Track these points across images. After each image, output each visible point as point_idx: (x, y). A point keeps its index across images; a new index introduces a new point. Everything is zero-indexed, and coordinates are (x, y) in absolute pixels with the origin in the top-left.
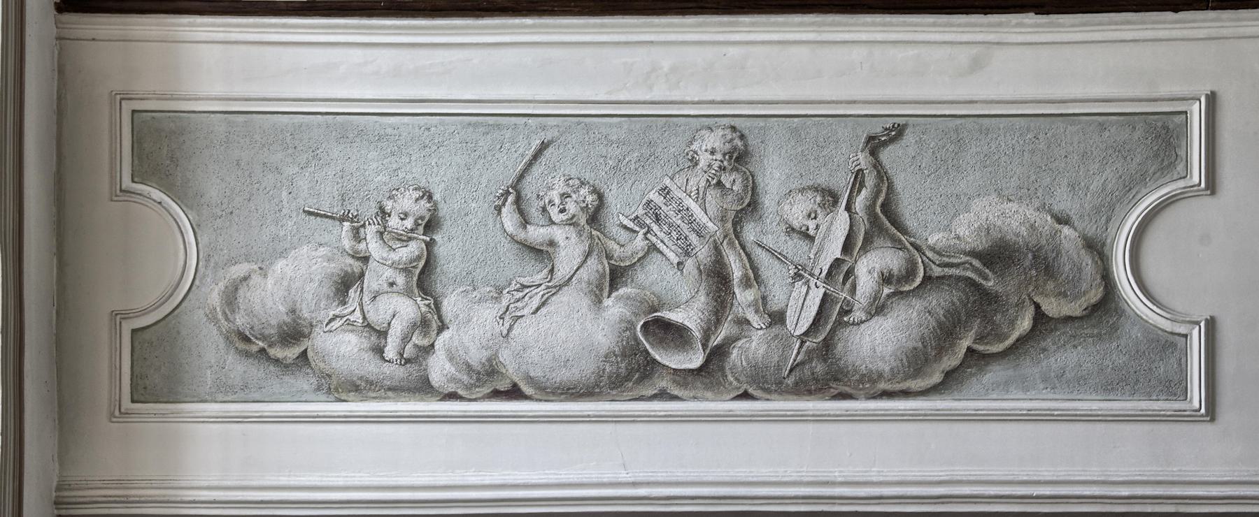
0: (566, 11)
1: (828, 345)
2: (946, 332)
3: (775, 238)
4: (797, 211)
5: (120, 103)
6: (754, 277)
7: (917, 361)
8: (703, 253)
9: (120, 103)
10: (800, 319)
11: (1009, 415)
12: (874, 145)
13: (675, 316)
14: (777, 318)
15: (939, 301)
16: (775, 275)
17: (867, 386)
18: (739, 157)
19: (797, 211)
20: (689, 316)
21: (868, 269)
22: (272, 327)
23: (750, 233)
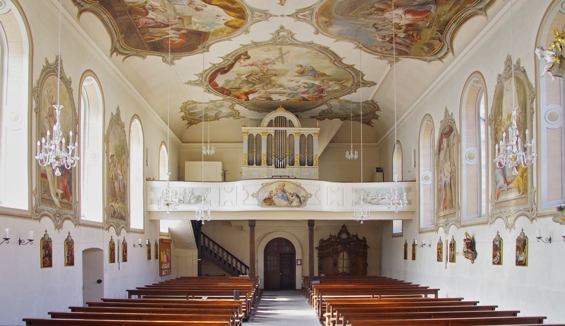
0: (466, 11)
1: (190, 201)
2: (196, 201)
3: (187, 195)
4: (188, 193)
5: (290, 274)
6: (186, 197)
7: (195, 202)
8: (183, 196)
9: (290, 274)
10: (188, 200)
11: (416, 310)
12: (192, 189)
13: (181, 199)
14: (187, 200)
15: (196, 199)
16: (187, 197)
17: (322, 275)
18: (185, 190)
19: (188, 193)
20: (182, 199)
21: (192, 197)
22: (242, 58)
23: (186, 194)
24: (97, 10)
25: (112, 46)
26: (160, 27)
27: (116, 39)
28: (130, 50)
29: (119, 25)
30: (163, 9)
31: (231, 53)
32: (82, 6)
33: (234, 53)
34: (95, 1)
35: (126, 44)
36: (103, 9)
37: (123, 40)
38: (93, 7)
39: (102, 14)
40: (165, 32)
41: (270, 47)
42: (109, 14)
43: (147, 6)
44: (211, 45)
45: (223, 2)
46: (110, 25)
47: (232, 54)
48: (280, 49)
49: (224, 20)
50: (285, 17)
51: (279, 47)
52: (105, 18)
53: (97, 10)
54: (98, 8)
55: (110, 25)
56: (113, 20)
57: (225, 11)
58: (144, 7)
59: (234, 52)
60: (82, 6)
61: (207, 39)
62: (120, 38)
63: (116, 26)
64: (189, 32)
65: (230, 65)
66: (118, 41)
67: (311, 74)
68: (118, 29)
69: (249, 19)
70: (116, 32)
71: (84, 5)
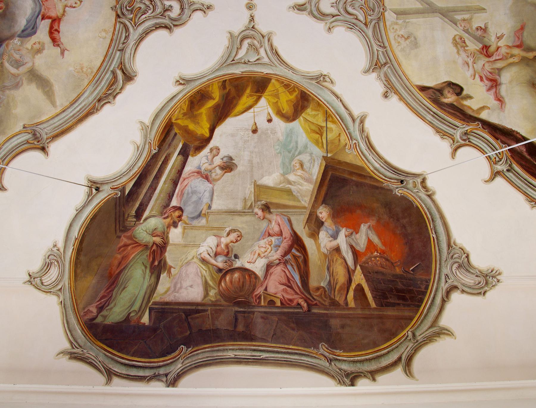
24: (202, 358)
25: (333, 377)
26: (306, 261)
27: (324, 363)
28: (389, 352)
29: (276, 337)
30: (228, 234)
31: (430, 124)
32: (166, 375)
33: (429, 117)
34: (177, 352)
35: (364, 350)
36: (208, 348)
37: (338, 352)
38: (190, 360)
39: (221, 356)
40: (326, 256)
41: (391, 36)
42: (230, 344)
43: (220, 262)
44: (386, 162)
45: (201, 113)
46: (264, 355)
47: (436, 123)
48: (400, 13)
49: (270, 121)
50: (247, 14)
51: (390, 16)
52: (235, 355)
53: (202, 358)
54: (197, 354)
55: (264, 355)
56: (254, 343)
57: (240, 107)
58: (223, 273)
59: (423, 118)
60: (166, 375)
61: (362, 168)
62: (327, 354)
63: (278, 345)
64: (324, 202)
65: (497, 135)
66: (330, 361)
67: (299, 174)
68: (291, 347)
69: (266, 71)
70: (296, 354)
71: (168, 372)
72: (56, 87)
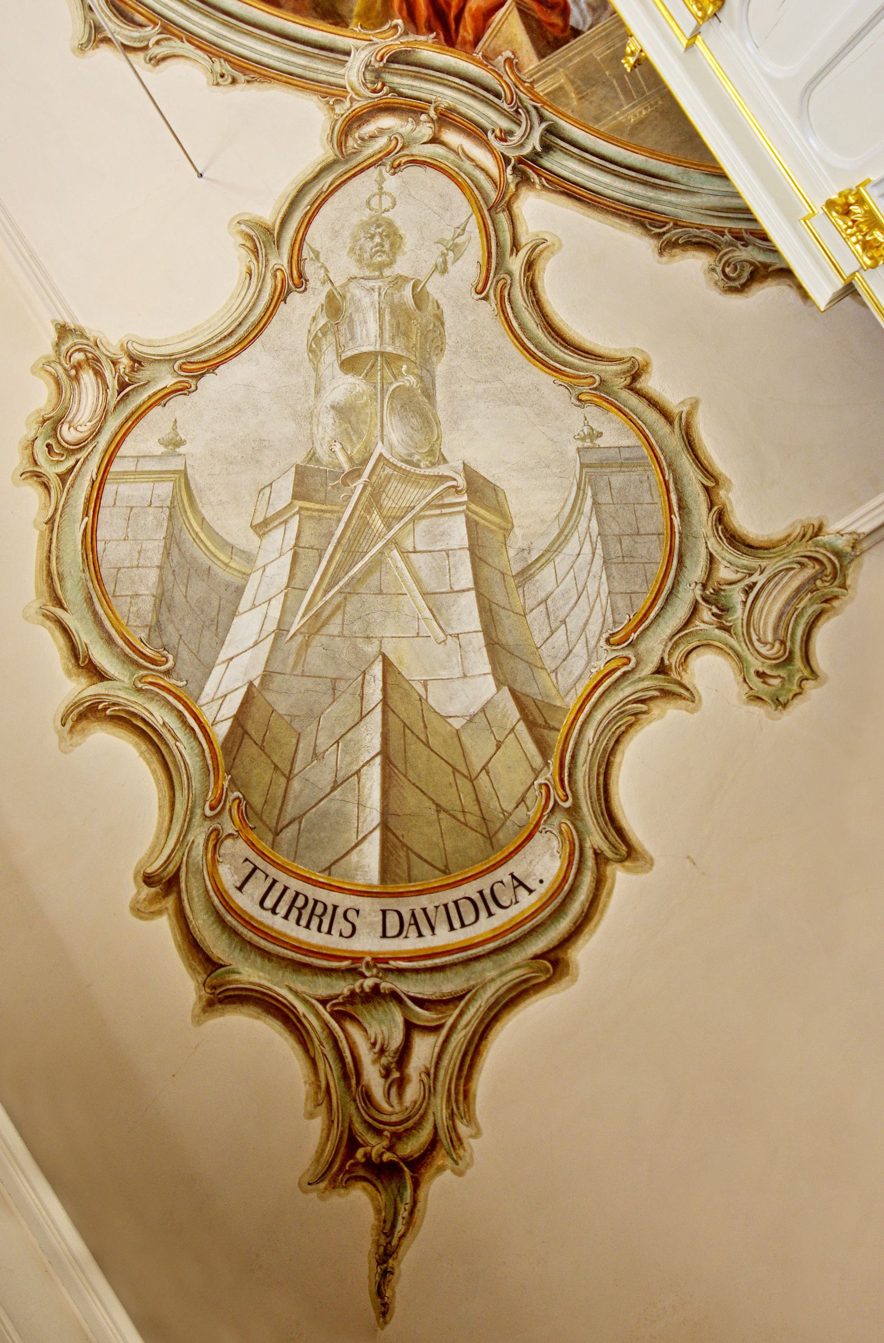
44: (306, 1050)
72: (764, 698)
